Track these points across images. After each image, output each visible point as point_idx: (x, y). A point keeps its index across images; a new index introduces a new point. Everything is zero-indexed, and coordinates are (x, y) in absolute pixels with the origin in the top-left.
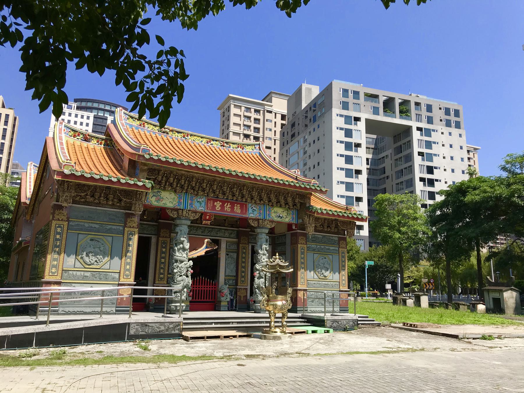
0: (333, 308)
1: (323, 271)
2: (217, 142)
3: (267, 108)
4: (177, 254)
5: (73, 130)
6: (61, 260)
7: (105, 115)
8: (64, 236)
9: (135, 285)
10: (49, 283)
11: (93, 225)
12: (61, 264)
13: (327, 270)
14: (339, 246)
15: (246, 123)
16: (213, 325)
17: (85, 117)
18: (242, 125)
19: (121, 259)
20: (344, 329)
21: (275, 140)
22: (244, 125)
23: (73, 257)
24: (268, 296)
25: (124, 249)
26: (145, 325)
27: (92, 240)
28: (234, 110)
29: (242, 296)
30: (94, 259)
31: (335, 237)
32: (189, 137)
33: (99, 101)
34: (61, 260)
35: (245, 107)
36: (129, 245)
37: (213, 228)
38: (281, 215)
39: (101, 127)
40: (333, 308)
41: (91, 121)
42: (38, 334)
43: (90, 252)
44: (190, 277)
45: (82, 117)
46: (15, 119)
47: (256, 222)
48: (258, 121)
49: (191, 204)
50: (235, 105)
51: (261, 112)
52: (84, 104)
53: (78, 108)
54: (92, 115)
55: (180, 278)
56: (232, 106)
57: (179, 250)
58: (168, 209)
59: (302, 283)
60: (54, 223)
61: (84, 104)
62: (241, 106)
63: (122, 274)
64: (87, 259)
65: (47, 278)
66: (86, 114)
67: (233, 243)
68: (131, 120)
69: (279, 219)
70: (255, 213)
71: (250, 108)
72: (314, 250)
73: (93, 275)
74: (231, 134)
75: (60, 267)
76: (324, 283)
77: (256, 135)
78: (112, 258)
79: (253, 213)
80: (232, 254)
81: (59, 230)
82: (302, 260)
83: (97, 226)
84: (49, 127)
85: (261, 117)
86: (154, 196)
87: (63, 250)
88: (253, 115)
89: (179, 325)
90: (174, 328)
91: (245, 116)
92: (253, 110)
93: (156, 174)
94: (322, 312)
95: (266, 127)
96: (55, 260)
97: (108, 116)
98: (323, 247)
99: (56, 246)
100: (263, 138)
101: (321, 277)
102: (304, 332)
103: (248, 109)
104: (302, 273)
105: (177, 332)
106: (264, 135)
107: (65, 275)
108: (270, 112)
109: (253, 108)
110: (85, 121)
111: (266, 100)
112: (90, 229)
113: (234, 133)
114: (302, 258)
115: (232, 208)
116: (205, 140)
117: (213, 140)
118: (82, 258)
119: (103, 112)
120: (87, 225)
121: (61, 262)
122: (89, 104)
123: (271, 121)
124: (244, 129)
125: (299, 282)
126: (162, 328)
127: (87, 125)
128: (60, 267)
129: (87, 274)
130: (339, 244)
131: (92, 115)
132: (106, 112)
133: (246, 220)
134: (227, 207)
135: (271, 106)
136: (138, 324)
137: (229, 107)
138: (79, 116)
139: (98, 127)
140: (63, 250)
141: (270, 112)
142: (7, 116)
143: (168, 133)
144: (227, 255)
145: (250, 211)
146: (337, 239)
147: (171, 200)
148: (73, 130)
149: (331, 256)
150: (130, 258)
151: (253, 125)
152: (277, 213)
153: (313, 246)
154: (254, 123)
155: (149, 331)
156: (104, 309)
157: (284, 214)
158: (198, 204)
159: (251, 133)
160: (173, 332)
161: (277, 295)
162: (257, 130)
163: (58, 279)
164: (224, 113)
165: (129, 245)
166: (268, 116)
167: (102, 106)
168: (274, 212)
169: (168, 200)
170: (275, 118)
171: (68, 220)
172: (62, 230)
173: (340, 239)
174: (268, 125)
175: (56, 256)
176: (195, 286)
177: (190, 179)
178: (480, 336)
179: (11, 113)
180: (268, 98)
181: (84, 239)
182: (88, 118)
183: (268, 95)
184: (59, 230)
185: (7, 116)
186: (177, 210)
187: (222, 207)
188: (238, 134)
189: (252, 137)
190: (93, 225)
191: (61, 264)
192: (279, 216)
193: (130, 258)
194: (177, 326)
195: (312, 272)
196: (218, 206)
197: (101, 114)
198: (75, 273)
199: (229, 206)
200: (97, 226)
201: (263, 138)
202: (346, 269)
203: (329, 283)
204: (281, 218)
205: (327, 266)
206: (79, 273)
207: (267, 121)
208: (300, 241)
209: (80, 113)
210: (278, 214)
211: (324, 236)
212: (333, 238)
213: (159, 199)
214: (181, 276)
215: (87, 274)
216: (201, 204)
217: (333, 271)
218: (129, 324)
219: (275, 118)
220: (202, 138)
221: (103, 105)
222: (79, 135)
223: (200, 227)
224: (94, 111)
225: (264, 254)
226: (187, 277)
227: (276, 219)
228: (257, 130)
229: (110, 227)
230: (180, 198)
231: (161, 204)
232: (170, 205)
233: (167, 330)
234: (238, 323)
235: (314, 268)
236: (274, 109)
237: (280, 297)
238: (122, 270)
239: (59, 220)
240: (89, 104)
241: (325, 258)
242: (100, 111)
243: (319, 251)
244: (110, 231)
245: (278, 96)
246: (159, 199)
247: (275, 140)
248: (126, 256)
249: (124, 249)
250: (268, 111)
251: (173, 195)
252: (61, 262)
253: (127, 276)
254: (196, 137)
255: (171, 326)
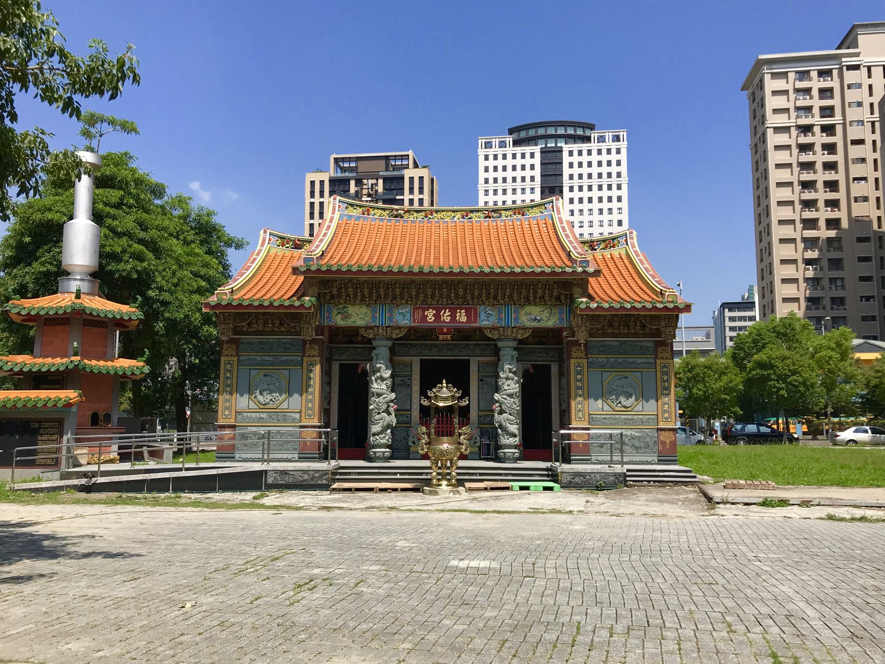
0: (611, 456)
1: (622, 399)
2: (478, 214)
3: (847, 61)
4: (375, 385)
5: (281, 238)
6: (234, 401)
7: (559, 145)
8: (235, 373)
9: (320, 427)
10: (223, 427)
11: (267, 358)
12: (233, 406)
13: (629, 396)
14: (656, 355)
15: (800, 103)
16: (398, 476)
17: (528, 155)
18: (792, 110)
19: (301, 395)
20: (597, 487)
21: (873, 123)
22: (798, 109)
23: (246, 396)
24: (429, 437)
25: (304, 383)
26: (284, 473)
27: (265, 376)
28: (771, 84)
29: (668, 442)
30: (269, 397)
31: (648, 342)
32: (435, 215)
33: (535, 124)
34: (234, 401)
35: (796, 72)
36: (310, 378)
37: (455, 345)
38: (538, 317)
39: (554, 166)
40: (611, 456)
41: (537, 161)
42: (174, 478)
43: (264, 390)
44: (393, 414)
45: (523, 156)
46: (432, 180)
47: (496, 332)
48: (829, 94)
49: (390, 318)
50: (772, 74)
51: (835, 73)
52: (523, 134)
53: (516, 143)
54: (537, 149)
55: (378, 417)
56: (767, 77)
57: (376, 380)
58: (361, 327)
59: (579, 418)
60: (223, 359)
61: (523, 134)
62: (787, 73)
63: (303, 415)
64: (261, 398)
65: (221, 422)
66: (527, 150)
67: (488, 364)
68: (350, 208)
69: (535, 324)
70: (492, 319)
71: (808, 72)
72: (603, 366)
73: (270, 417)
74: (770, 132)
75: (234, 409)
76: (623, 417)
77: (828, 121)
78: (290, 395)
79: (487, 318)
80: (487, 379)
81: (228, 367)
82: (579, 384)
83: (270, 359)
84: (478, 183)
85: (834, 83)
86: (339, 313)
87: (234, 389)
88: (816, 84)
89: (327, 474)
90: (320, 478)
91: (797, 91)
92: (814, 74)
93: (329, 287)
94: (605, 463)
95: (847, 101)
96: (227, 401)
97: (563, 145)
98: (620, 360)
99: (227, 386)
100: (844, 124)
101: (617, 409)
102: (507, 488)
103: (804, 75)
104: (579, 403)
105: (324, 482)
106: (844, 119)
107: (239, 417)
108: (856, 67)
109: (813, 70)
110: (528, 161)
111: (846, 44)
112: (263, 364)
113: (775, 128)
114: (578, 381)
115: (453, 316)
116: (459, 215)
117: (472, 212)
118: (255, 397)
119: (554, 140)
120: (258, 358)
121: (234, 403)
122: (532, 133)
123: (859, 86)
124: (798, 117)
125: (573, 417)
126: (306, 477)
127: (532, 167)
128: (234, 409)
129: (263, 415)
130: (656, 351)
131: (537, 149)
132: (559, 140)
133: (480, 330)
134: (446, 316)
135: (857, 55)
136: (276, 471)
137: (762, 81)
138: (519, 156)
139: (549, 166)
140: (234, 389)
141: (856, 67)
142: (421, 179)
143: (402, 217)
144: (482, 380)
145: (483, 316)
146: (652, 344)
147: (362, 316)
148: (281, 238)
149: (638, 375)
150: (312, 394)
151: (817, 103)
152: (530, 314)
153: (602, 359)
154: (821, 98)
155: (289, 480)
156: (271, 456)
157: (546, 314)
158: (401, 317)
159: (816, 120)
160: (319, 482)
161: (438, 435)
162: (828, 112)
163: (231, 422)
164: (753, 93)
165: (310, 378)
166: (850, 77)
167: (551, 131)
168: (526, 314)
169: (358, 316)
170: (870, 76)
171: (238, 355)
172: (232, 367)
173: (659, 344)
174: (851, 96)
175: (228, 397)
176: (441, 426)
177: (390, 286)
178: (760, 500)
179: (424, 173)
180: (849, 40)
181: (256, 374)
182: (532, 155)
183: (848, 35)
184: (228, 367)
185: (421, 179)
186: (371, 328)
187: (453, 316)
188: (786, 129)
189: (817, 129)
190: (267, 358)
191: (233, 406)
192: (536, 319)
193: (311, 394)
194: (325, 475)
195: (600, 401)
196: (430, 317)
197: (551, 145)
198: (249, 414)
199: (448, 313)
200: (270, 359)
201: (844, 124)
202: (672, 392)
203: (636, 417)
204: (539, 321)
205: (630, 390)
206: (254, 415)
207: (850, 106)
208: (574, 355)
209: (519, 150)
210: (533, 317)
211: (622, 343)
212: (645, 344)
213: (346, 317)
214: (379, 413)
215: (263, 415)
216: (404, 316)
217: (644, 396)
218: (266, 471)
219: (870, 76)
220: (454, 211)
221: (553, 128)
222: (288, 243)
223: (435, 345)
224: (540, 141)
225: (507, 379)
226: (389, 414)
227: (528, 324)
228: (827, 112)
229: (285, 358)
230: (374, 311)
231: (349, 323)
232: (360, 323)
233: (312, 479)
234: (401, 474)
235: (602, 394)
236: (865, 59)
237: (445, 439)
238: (660, 412)
239: (227, 355)
240: (532, 133)
241: (626, 378)
242: (549, 140)
243: (612, 367)
244: (286, 363)
245: (872, 30)
246: (346, 317)
247: (873, 123)
248: (307, 391)
249: (304, 383)
250: (849, 68)
251: (364, 309)
252: (234, 403)
253: (310, 415)
254: (444, 213)
255: (317, 475)
